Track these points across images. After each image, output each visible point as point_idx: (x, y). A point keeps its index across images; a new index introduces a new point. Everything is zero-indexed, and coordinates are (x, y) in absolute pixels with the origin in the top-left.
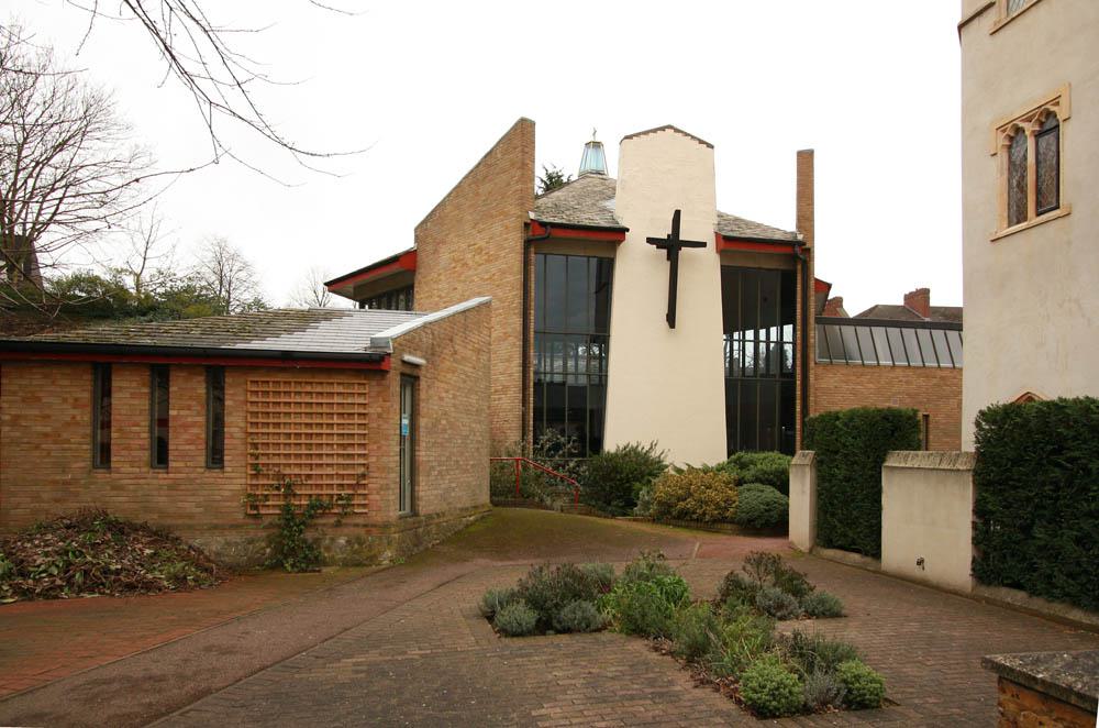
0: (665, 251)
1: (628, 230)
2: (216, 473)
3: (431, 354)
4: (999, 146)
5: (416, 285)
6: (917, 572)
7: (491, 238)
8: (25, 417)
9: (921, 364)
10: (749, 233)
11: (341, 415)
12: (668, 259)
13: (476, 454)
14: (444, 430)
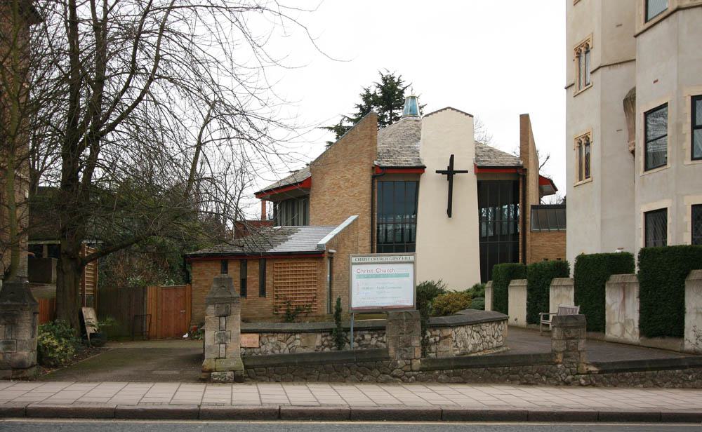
0: (446, 176)
2: (263, 298)
3: (337, 248)
5: (311, 196)
8: (200, 280)
11: (307, 274)
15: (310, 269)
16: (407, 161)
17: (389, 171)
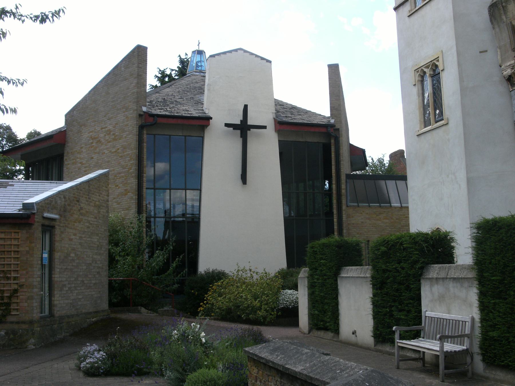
0: (239, 132)
1: (211, 118)
4: (417, 80)
5: (65, 154)
6: (353, 338)
7: (117, 124)
9: (399, 205)
10: (298, 119)
12: (241, 137)
13: (97, 276)
14: (73, 260)
15: (9, 243)
16: (188, 111)
17: (160, 120)
